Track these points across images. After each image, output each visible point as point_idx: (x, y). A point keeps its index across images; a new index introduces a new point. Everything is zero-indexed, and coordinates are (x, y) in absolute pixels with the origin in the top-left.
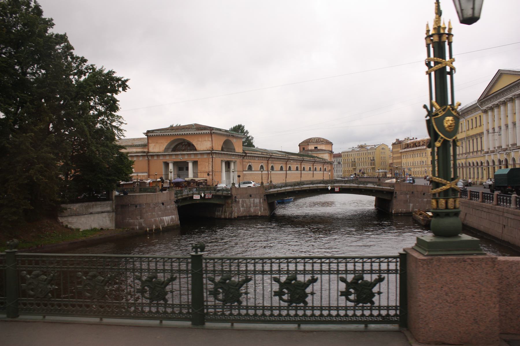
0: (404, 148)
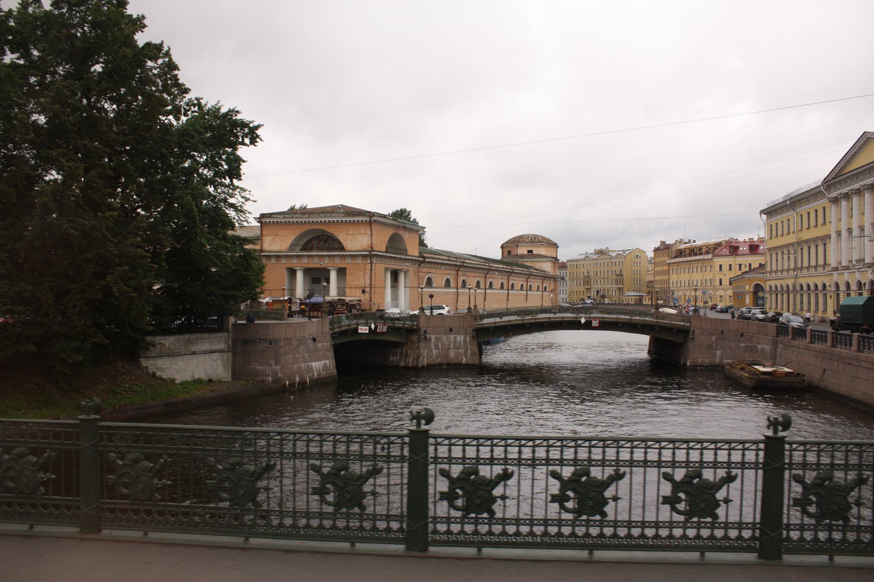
0: (673, 256)
